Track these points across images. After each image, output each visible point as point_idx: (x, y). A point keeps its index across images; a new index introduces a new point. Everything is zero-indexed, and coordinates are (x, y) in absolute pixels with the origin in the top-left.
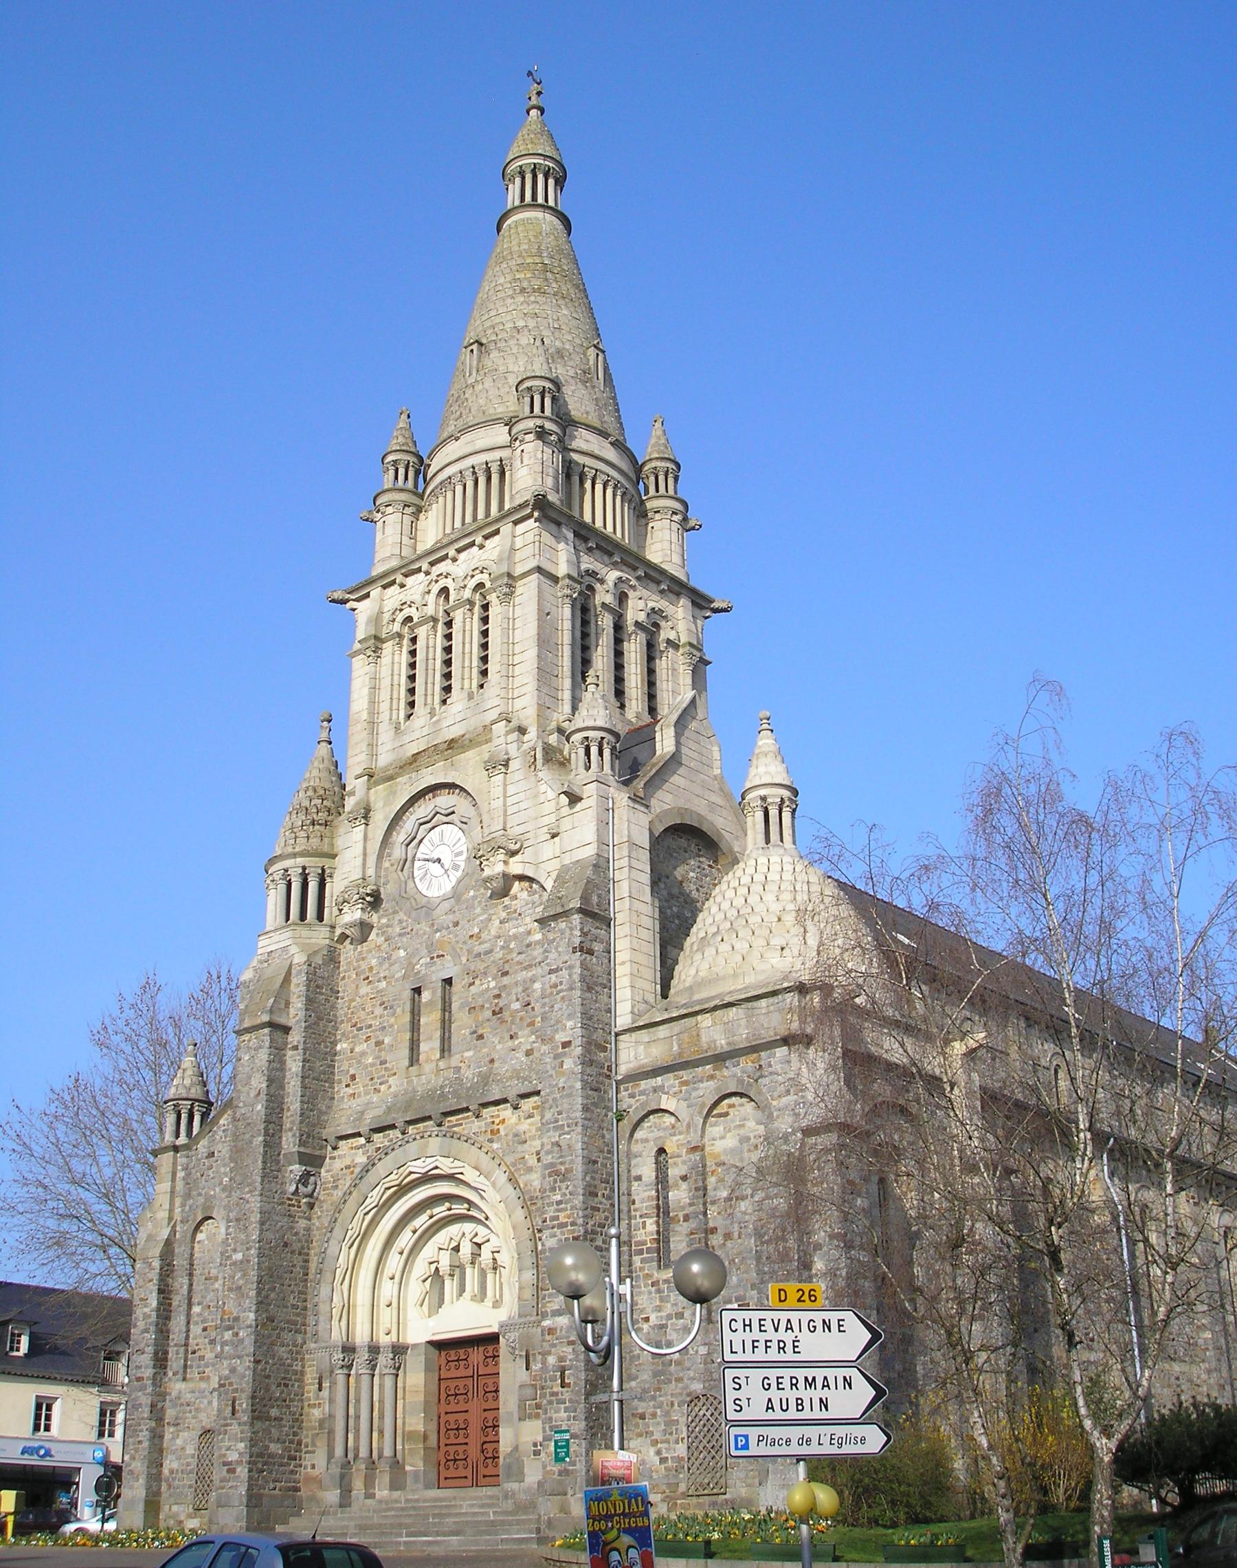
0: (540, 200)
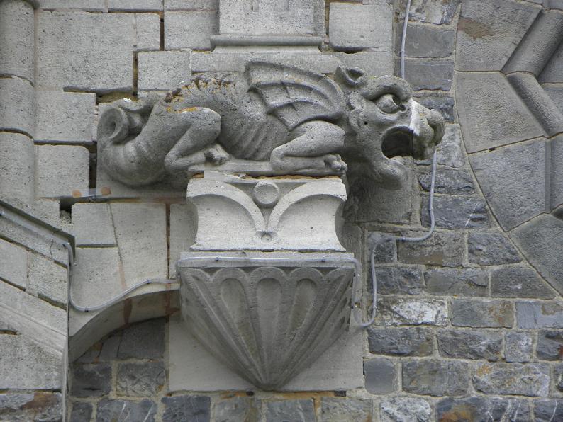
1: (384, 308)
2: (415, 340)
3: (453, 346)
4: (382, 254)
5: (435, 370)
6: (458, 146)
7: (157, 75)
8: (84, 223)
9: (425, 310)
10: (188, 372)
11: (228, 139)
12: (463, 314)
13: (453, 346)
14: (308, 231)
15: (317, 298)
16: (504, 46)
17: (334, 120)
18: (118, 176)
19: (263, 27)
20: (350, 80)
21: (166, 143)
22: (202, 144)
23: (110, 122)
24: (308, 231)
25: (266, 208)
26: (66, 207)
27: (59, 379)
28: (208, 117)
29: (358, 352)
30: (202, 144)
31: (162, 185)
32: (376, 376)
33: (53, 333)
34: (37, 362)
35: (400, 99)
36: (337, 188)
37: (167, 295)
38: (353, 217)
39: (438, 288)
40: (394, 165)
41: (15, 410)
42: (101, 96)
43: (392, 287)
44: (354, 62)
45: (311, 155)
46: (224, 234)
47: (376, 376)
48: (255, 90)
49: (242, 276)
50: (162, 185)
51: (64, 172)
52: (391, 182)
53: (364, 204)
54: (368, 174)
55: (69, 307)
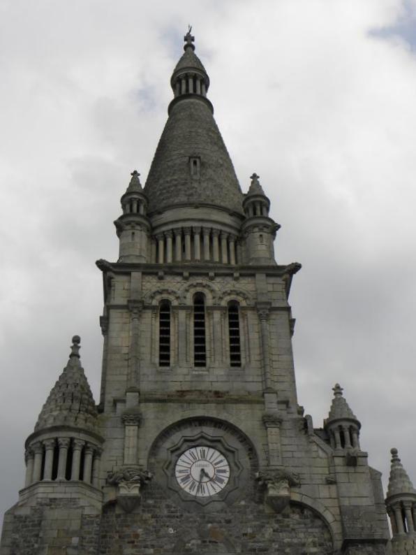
0: (191, 91)
1: (145, 501)
2: (149, 506)
3: (154, 506)
4: (145, 494)
5: (151, 510)
6: (85, 536)
7: (115, 469)
8: (105, 490)
9: (151, 502)
10: (118, 511)
11: (125, 478)
12: (155, 502)
13: (154, 506)
14: (135, 491)
15: (135, 500)
16: (162, 465)
17: (138, 475)
18: (109, 483)
19: (130, 463)
20: (141, 470)
21: (116, 479)
22: (121, 479)
23: (109, 476)
24: (135, 491)
25: (129, 488)
26: (103, 487)
27: (100, 513)
28: (122, 475)
29: (141, 508)
30: (121, 479)
31: (115, 485)
32: (143, 511)
33: (99, 506)
34: (254, 299)
35: (148, 473)
36: (139, 485)
37: (115, 500)
38: (141, 489)
39: (153, 498)
40: (147, 482)
41: (254, 308)
42: (108, 472)
43: (146, 498)
44: (141, 467)
45: (135, 480)
46: (123, 492)
47: (143, 511)
48: (128, 472)
49: (125, 498)
50: (115, 485)
51: (102, 483)
52: (146, 484)
53: (143, 487)
54: (144, 483)
55: (102, 502)
